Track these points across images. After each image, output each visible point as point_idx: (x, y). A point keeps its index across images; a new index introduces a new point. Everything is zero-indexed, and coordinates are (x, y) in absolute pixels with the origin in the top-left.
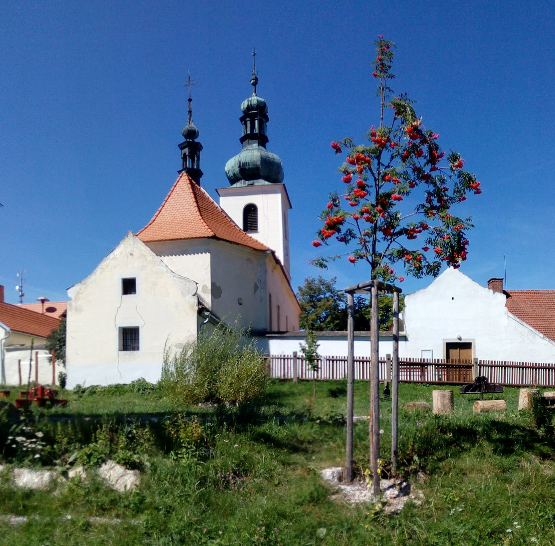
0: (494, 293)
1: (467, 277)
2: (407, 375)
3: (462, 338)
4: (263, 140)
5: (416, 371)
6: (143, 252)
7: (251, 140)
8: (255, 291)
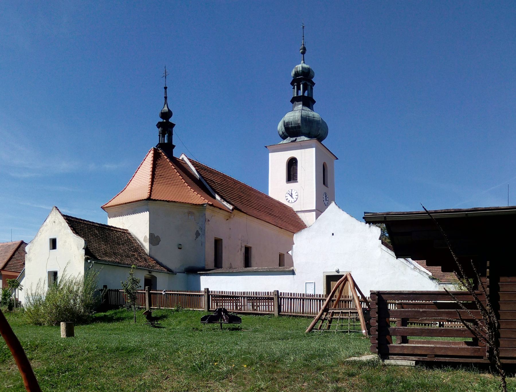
0: (370, 226)
1: (345, 213)
2: (233, 306)
4: (308, 102)
5: (262, 302)
7: (297, 102)
8: (197, 237)
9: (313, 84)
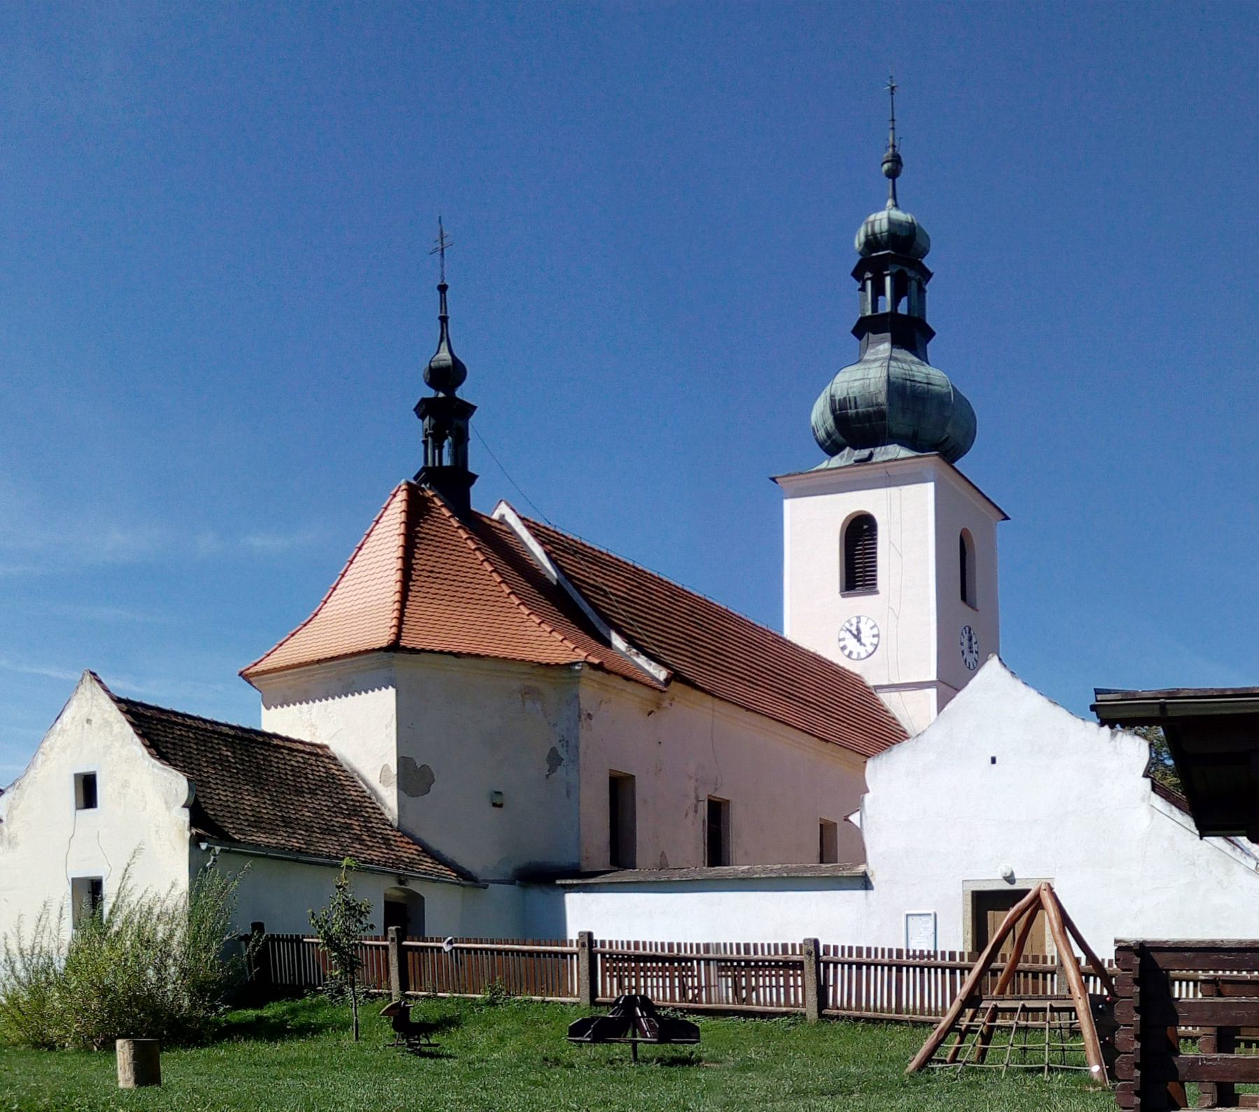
0: (1113, 735)
1: (1033, 692)
2: (664, 987)
3: (1016, 876)
4: (911, 334)
6: (106, 716)
7: (874, 333)
8: (552, 770)
9: (927, 275)
